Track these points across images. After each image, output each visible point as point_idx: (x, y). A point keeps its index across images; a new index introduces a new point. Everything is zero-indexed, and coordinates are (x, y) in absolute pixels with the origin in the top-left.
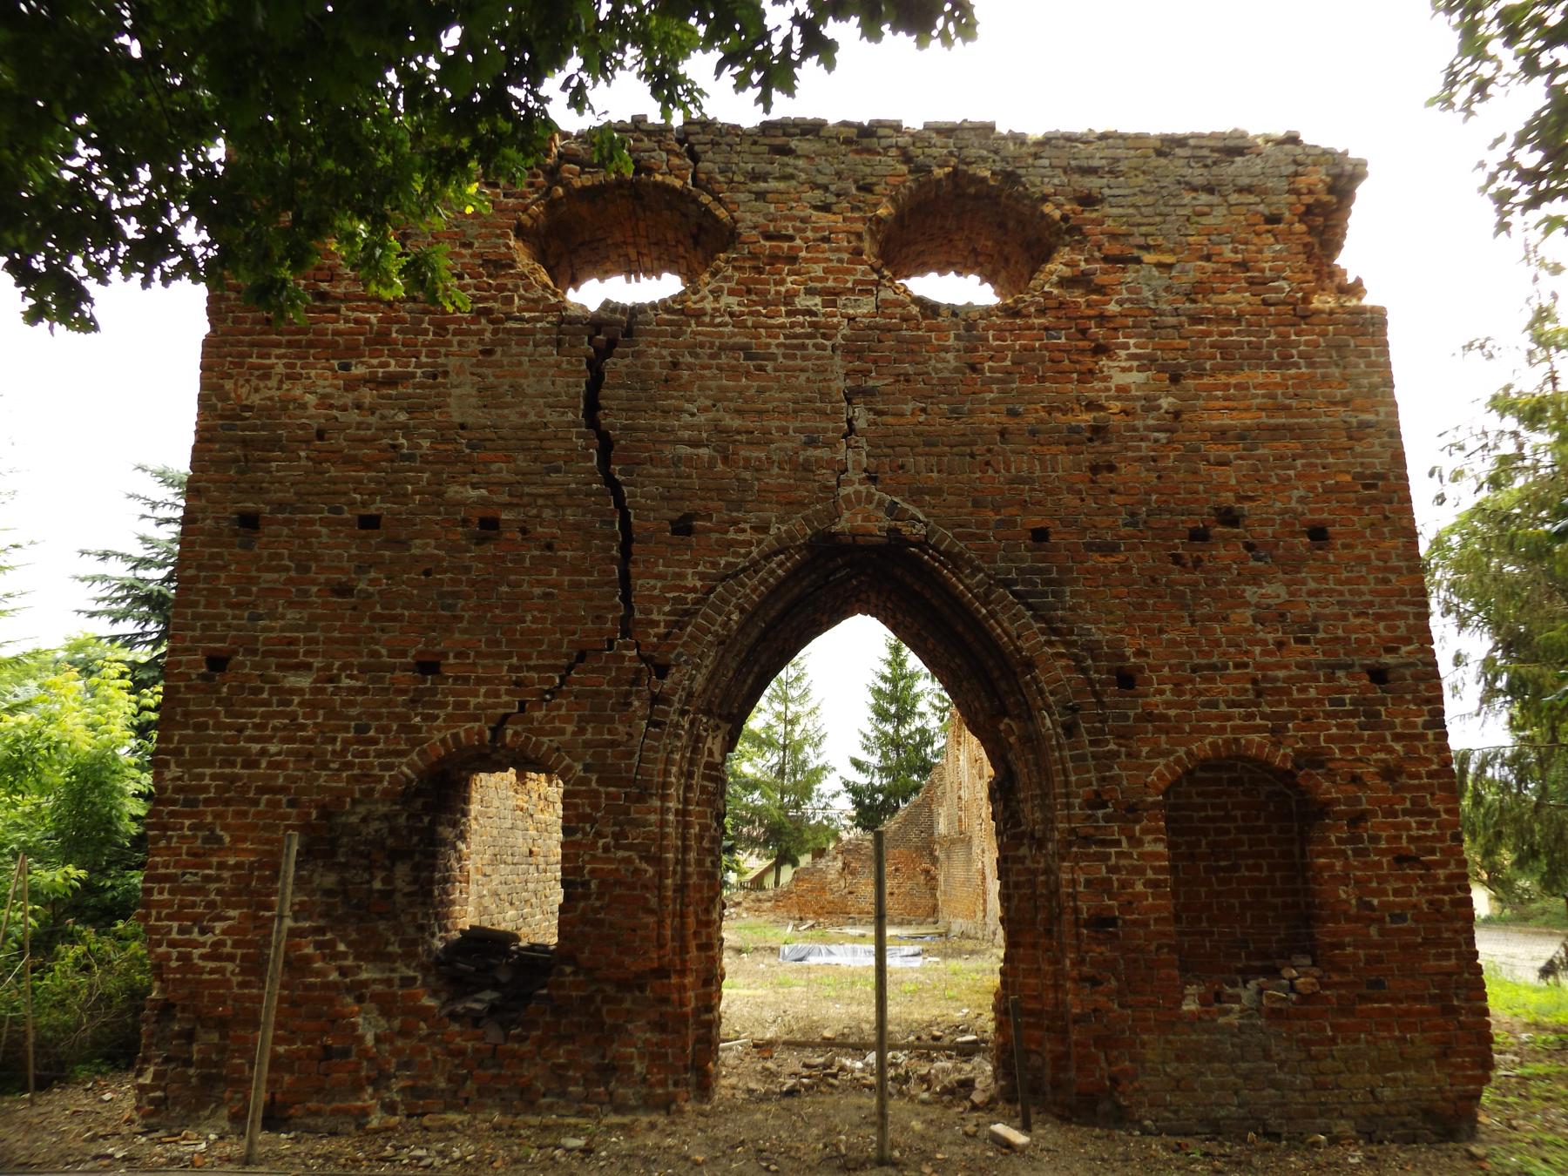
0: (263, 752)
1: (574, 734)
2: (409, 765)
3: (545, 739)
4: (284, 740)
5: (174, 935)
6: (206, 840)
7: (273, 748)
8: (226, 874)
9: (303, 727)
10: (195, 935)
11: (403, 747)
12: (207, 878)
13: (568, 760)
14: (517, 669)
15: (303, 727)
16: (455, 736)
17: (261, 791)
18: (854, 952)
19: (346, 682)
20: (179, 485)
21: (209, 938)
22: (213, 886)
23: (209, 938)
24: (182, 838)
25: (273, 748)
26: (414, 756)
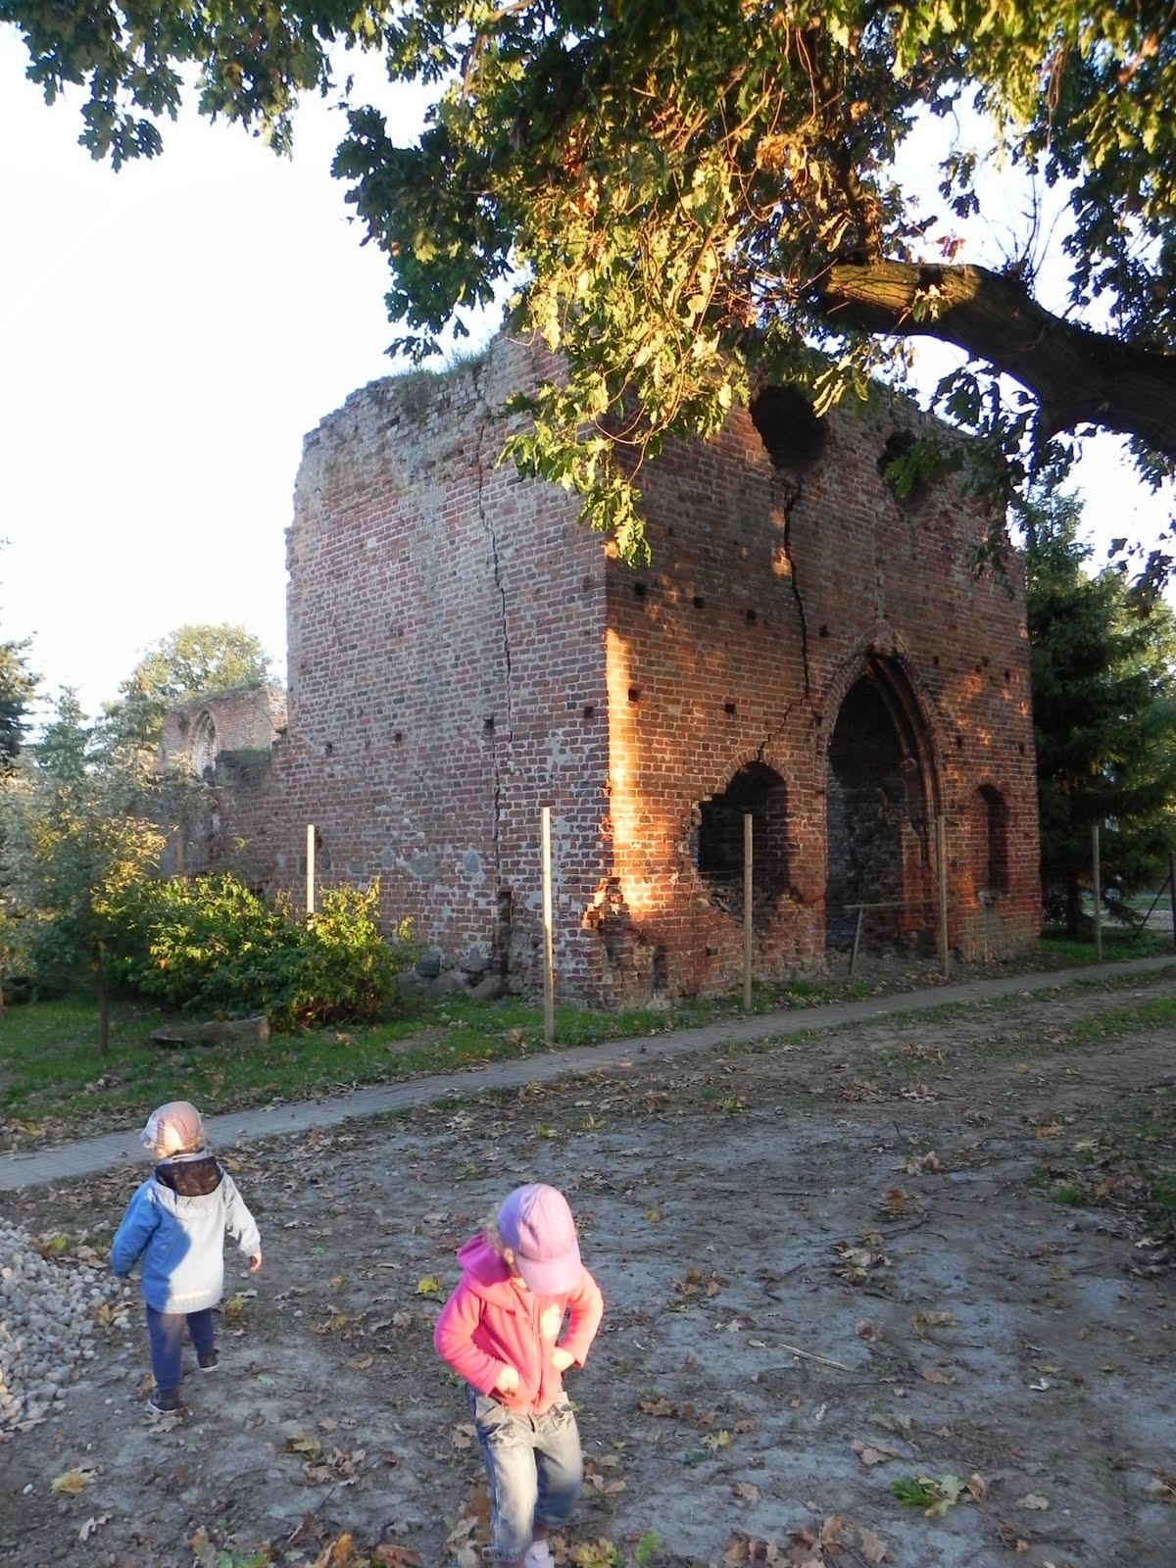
7: (667, 757)
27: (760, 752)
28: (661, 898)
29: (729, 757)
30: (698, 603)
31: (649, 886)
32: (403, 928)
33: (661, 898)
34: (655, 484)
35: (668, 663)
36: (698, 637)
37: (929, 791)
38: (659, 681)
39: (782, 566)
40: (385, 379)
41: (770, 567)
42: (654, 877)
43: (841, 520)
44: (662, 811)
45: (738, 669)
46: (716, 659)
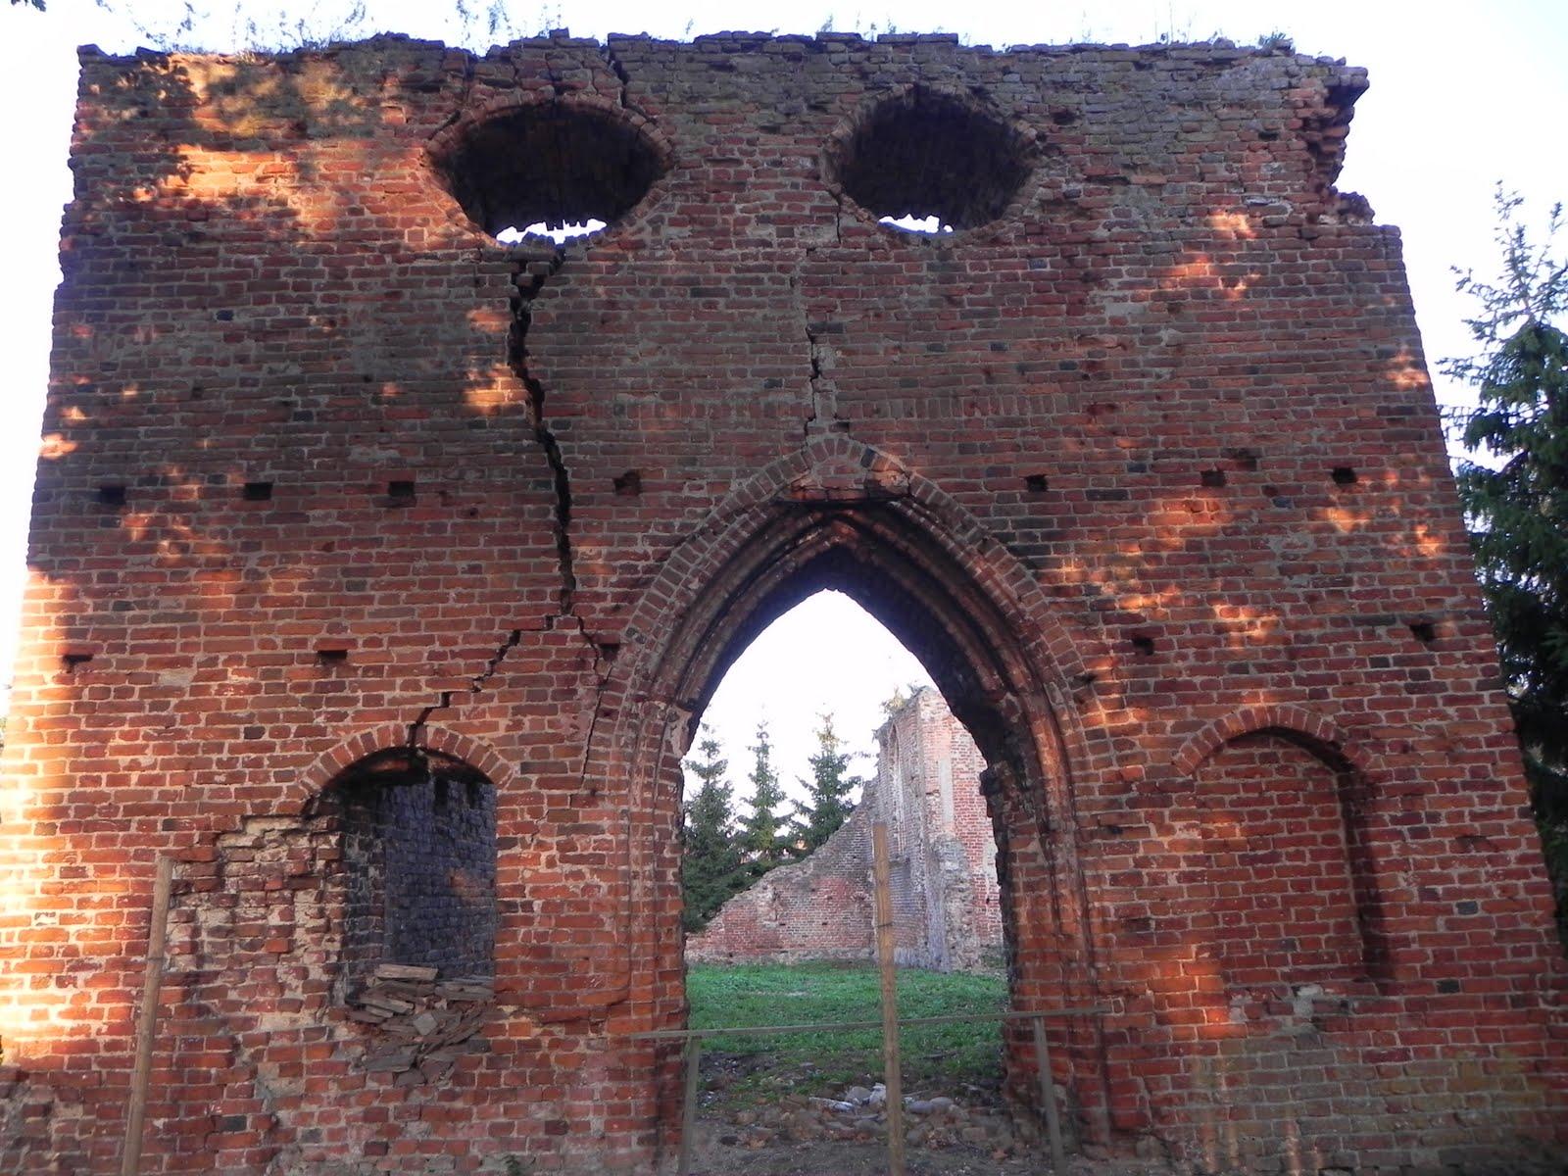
2: (310, 774)
7: (144, 760)
8: (89, 913)
9: (181, 734)
12: (65, 920)
13: (502, 760)
15: (181, 734)
16: (367, 738)
17: (129, 811)
19: (234, 679)
22: (72, 929)
27: (414, 729)
28: (97, 1014)
29: (315, 747)
30: (257, 492)
31: (69, 992)
32: (819, 197)
33: (97, 1014)
34: (165, 330)
35: (166, 601)
36: (247, 547)
37: (1049, 760)
38: (136, 634)
39: (495, 392)
40: (1417, 332)
41: (461, 398)
42: (82, 976)
43: (688, 282)
44: (123, 856)
45: (361, 586)
46: (290, 582)
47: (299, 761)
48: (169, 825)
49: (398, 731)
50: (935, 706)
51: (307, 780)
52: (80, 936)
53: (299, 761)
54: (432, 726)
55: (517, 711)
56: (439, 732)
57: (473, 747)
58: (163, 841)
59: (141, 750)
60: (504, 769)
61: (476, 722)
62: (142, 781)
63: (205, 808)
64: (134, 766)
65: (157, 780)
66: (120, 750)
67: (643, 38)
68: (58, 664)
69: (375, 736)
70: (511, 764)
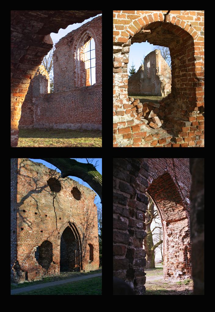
0: (28, 240)
1: (196, 20)
2: (130, 28)
3: (186, 21)
4: (30, 239)
5: (21, 262)
6: (23, 250)
7: (29, 240)
8: (25, 254)
9: (31, 237)
10: (23, 261)
11: (127, 19)
12: (24, 255)
13: (195, 30)
14: (49, 232)
15: (31, 237)
16: (150, 16)
17: (28, 245)
18: (58, 268)
19: (35, 232)
20: (12, 42)
21: (25, 262)
22: (24, 256)
23: (25, 262)
24: (21, 250)
25: (29, 240)
26: (132, 23)
47: (126, 23)
48: (31, 246)
49: (160, 16)
50: (59, 256)
51: (129, 30)
52: (25, 256)
53: (126, 23)
54: (48, 238)
55: (54, 238)
56: (174, 17)
57: (185, 24)
58: (31, 248)
59: (28, 239)
60: (195, 33)
61: (186, 16)
62: (29, 242)
63: (33, 245)
64: (28, 240)
65: (30, 242)
66: (27, 239)
67: (140, 42)
68: (16, 113)
69: (153, 17)
70: (198, 32)
